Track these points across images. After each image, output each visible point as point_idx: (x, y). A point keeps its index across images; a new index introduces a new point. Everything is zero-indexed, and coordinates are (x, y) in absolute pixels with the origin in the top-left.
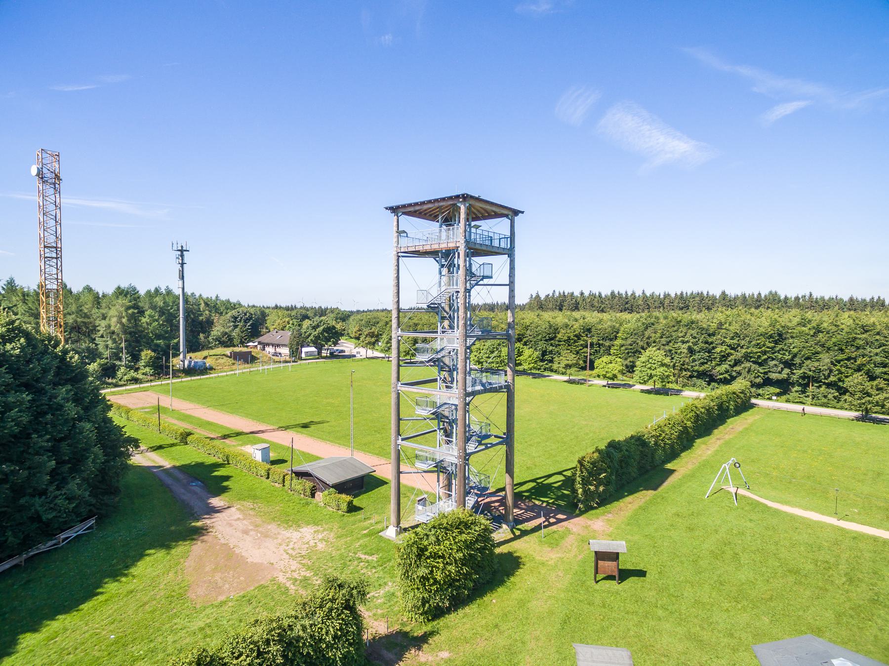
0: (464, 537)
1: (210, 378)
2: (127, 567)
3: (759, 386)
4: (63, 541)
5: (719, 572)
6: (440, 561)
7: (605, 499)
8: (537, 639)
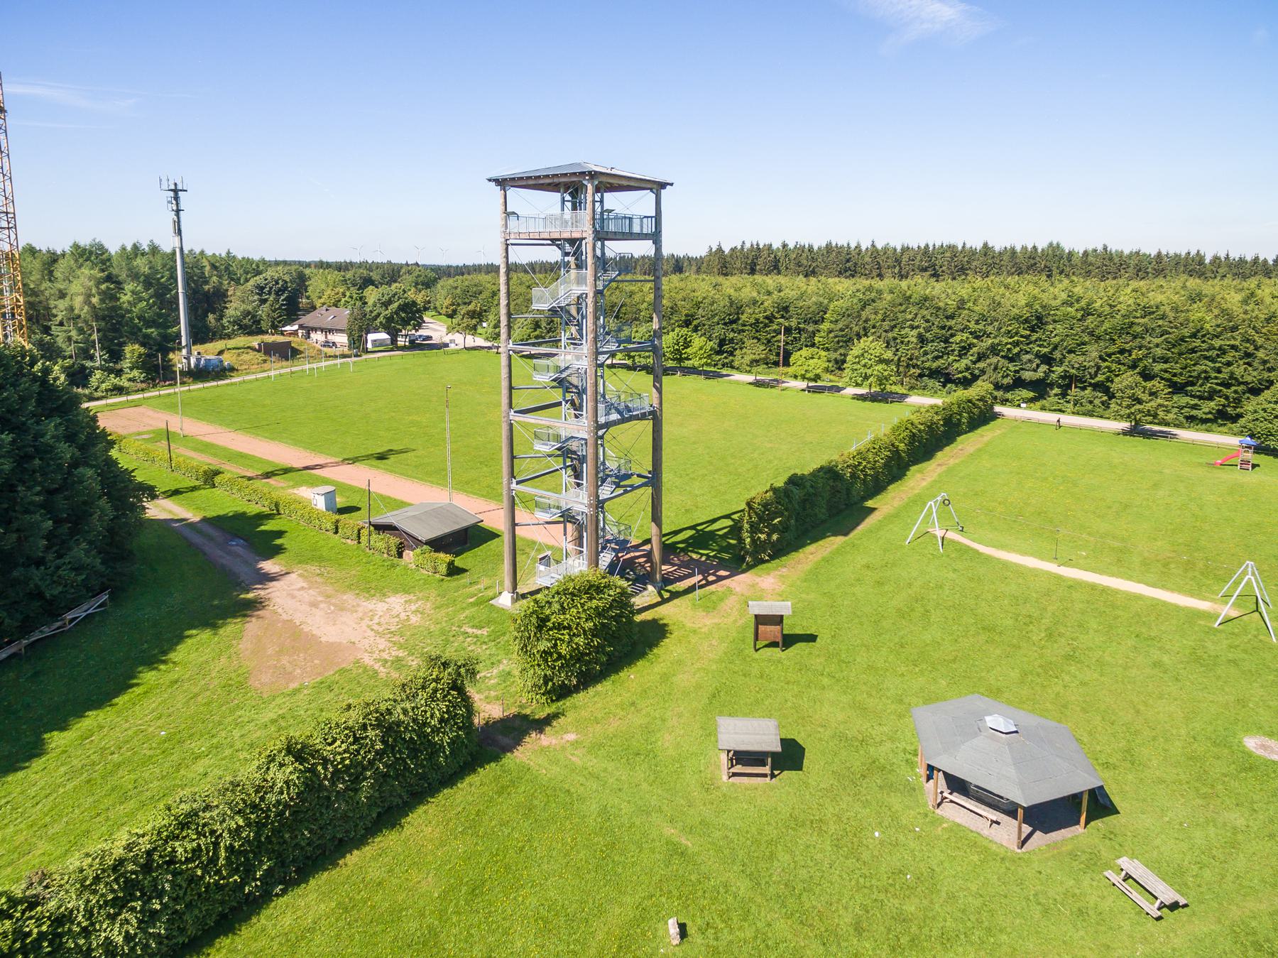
0: (594, 603)
1: (232, 384)
2: (165, 653)
3: (1008, 388)
4: (70, 623)
5: (901, 633)
6: (565, 632)
7: (780, 550)
8: (680, 715)
